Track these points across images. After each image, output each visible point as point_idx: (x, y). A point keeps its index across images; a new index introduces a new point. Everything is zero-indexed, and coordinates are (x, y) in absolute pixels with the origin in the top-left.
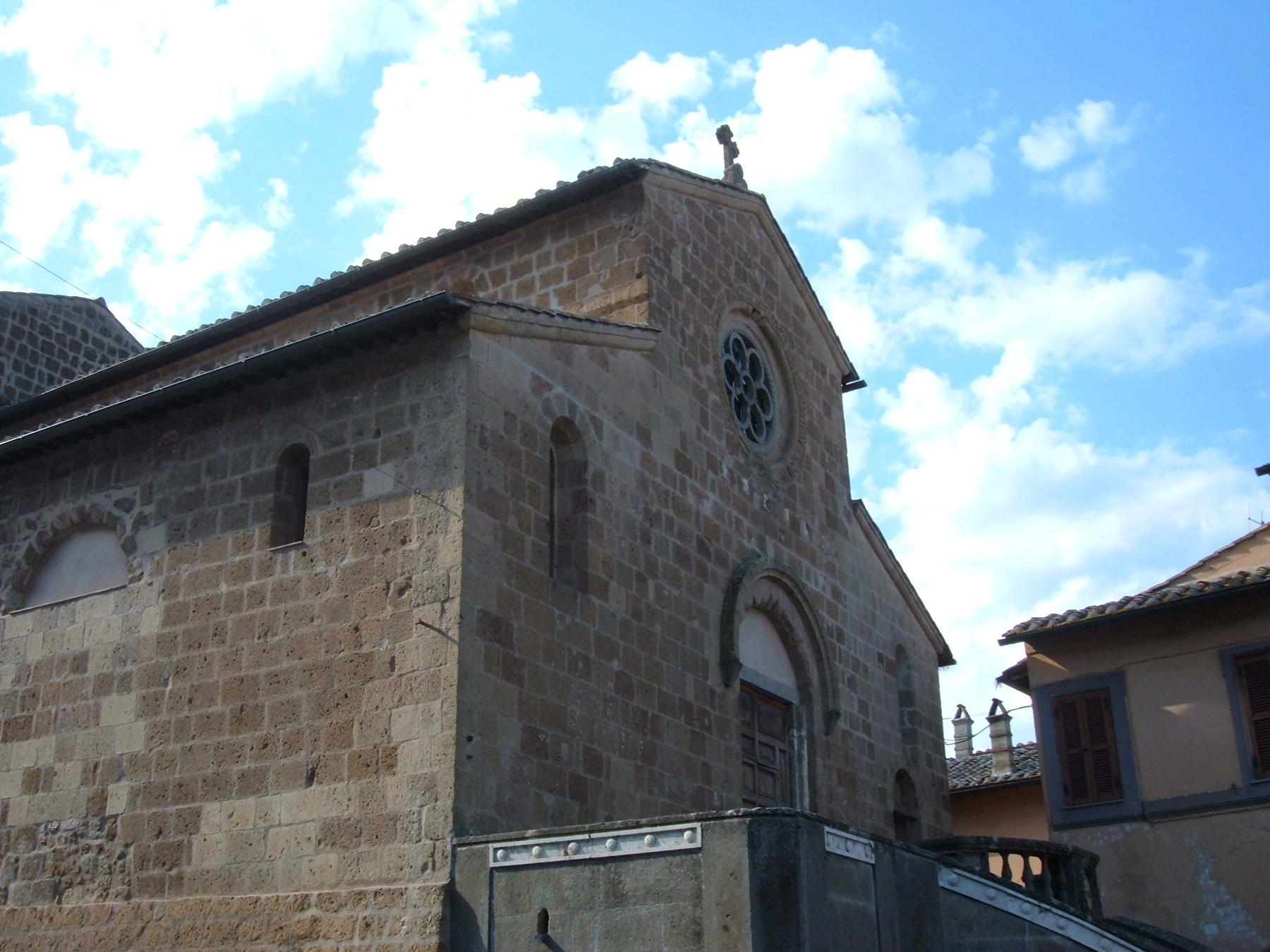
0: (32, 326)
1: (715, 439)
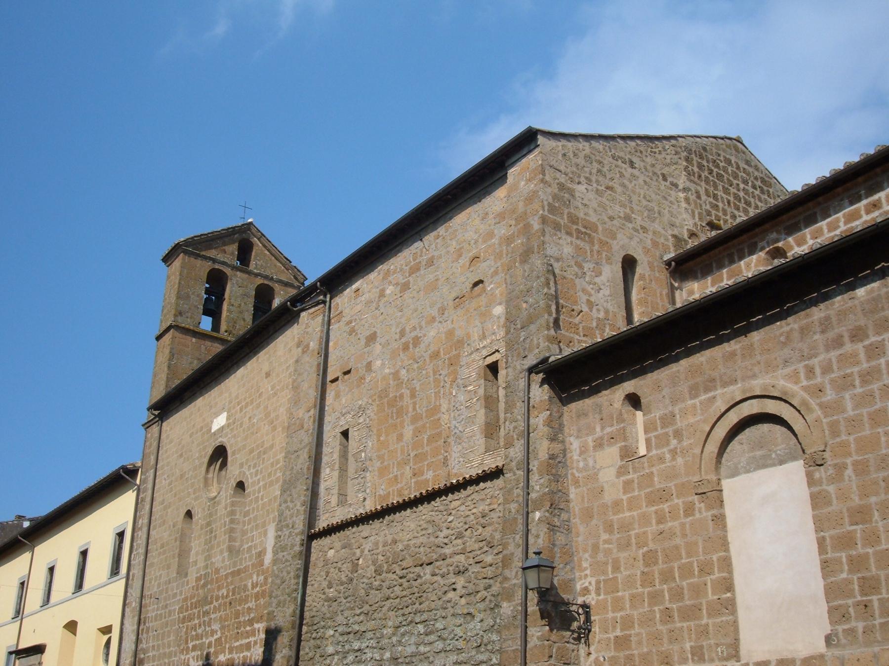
0: (708, 162)
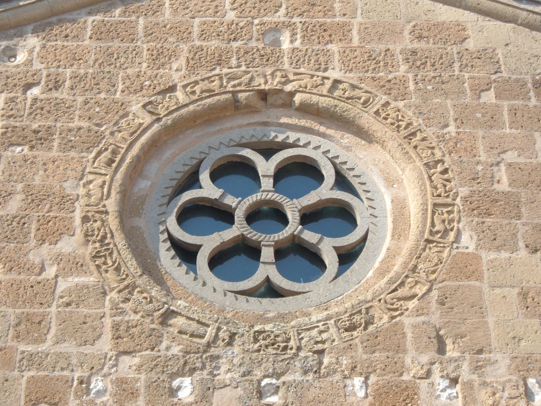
1: (69, 347)
